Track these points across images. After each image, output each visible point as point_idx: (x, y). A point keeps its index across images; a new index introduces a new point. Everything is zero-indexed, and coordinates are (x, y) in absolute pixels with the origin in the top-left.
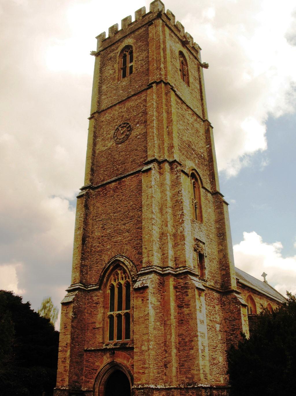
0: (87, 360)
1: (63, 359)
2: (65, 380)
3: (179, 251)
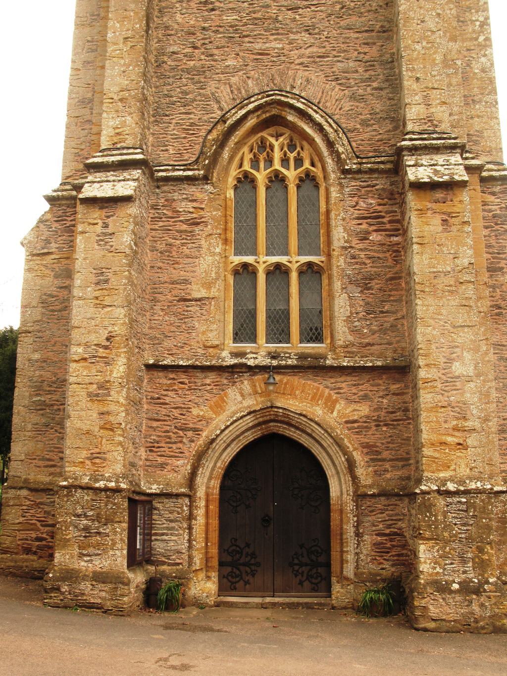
0: (152, 398)
1: (95, 386)
2: (107, 456)
3: (476, 119)
